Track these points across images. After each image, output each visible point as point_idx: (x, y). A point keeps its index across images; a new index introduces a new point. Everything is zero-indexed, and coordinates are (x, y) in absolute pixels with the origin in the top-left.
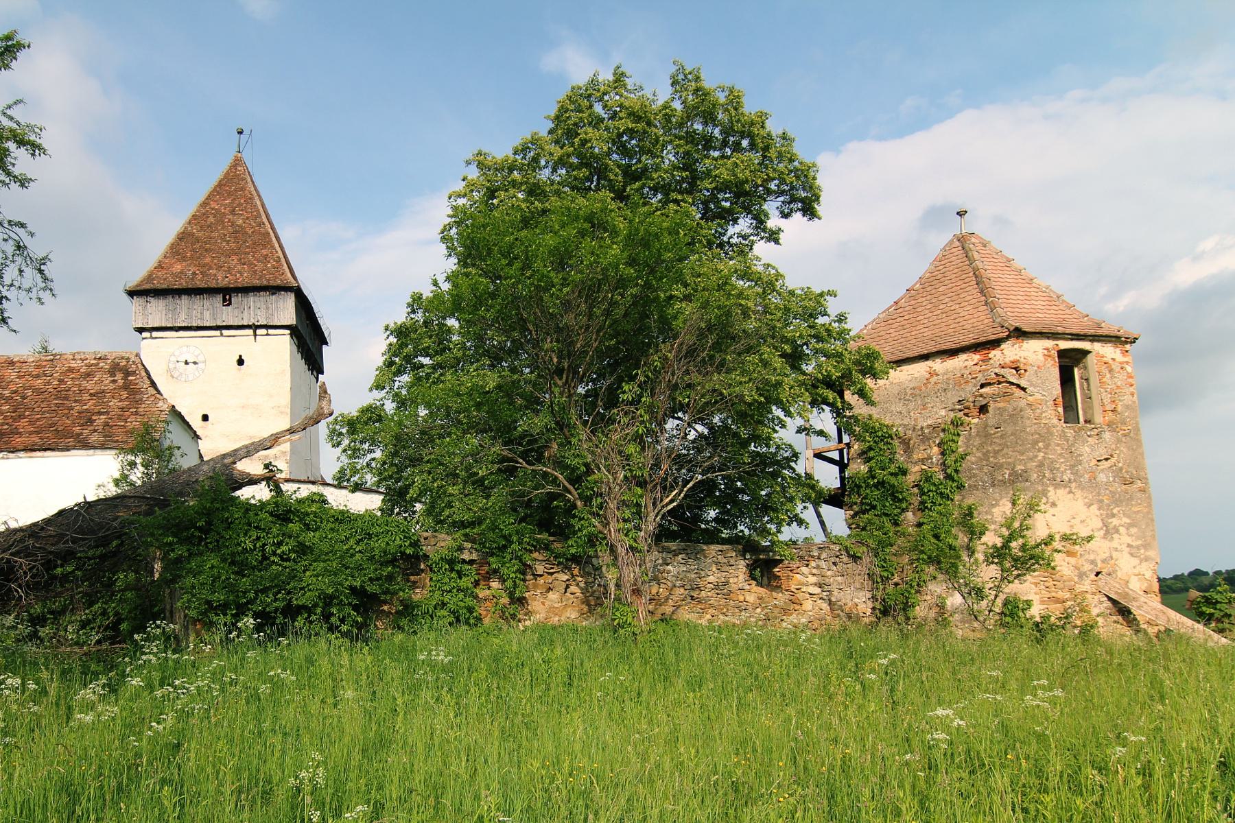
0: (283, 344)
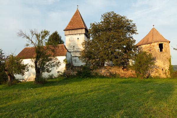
0: (83, 36)
